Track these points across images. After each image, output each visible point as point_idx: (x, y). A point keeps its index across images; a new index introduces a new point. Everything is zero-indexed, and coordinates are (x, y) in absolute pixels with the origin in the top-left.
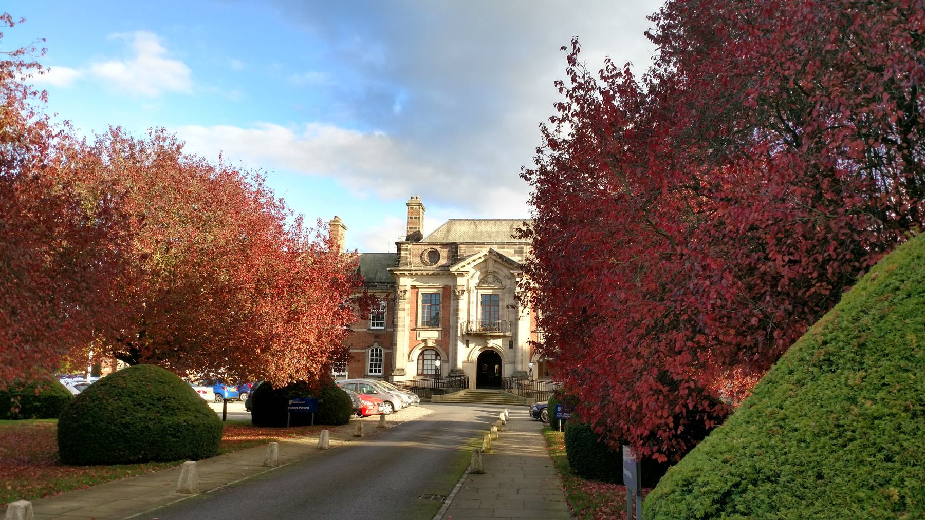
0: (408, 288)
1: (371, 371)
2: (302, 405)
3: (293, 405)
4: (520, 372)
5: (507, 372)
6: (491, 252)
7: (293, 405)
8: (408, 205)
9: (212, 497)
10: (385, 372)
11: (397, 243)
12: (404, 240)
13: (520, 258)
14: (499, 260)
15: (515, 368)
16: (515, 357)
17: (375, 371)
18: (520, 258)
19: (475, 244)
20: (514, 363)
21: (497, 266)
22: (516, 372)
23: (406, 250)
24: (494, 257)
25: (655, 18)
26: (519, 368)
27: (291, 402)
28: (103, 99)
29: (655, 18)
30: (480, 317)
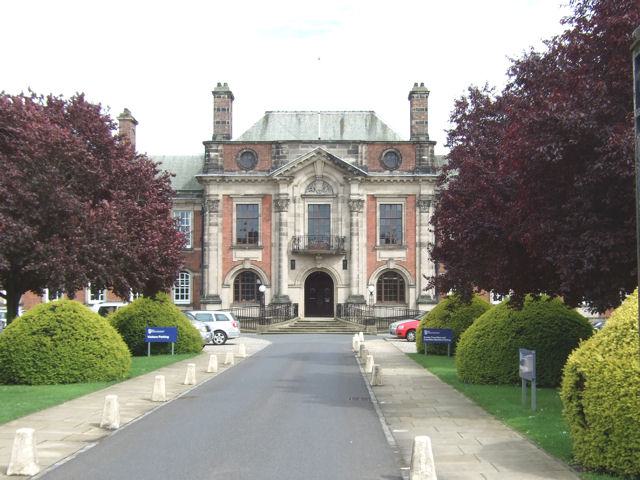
0: (220, 198)
1: (177, 297)
2: (162, 334)
3: (153, 334)
4: (355, 297)
5: (340, 296)
6: (319, 153)
7: (153, 334)
8: (214, 93)
9: (187, 401)
10: (194, 296)
11: (205, 143)
12: (211, 139)
13: (353, 160)
14: (330, 163)
15: (350, 292)
16: (350, 279)
17: (182, 297)
18: (353, 160)
19: (300, 142)
20: (349, 286)
21: (328, 169)
22: (350, 296)
23: (217, 151)
24: (324, 159)
25: (546, 42)
26: (355, 292)
27: (150, 331)
28: (630, 303)
29: (546, 42)
30: (307, 232)
